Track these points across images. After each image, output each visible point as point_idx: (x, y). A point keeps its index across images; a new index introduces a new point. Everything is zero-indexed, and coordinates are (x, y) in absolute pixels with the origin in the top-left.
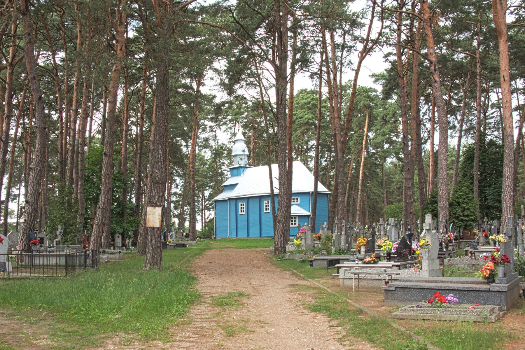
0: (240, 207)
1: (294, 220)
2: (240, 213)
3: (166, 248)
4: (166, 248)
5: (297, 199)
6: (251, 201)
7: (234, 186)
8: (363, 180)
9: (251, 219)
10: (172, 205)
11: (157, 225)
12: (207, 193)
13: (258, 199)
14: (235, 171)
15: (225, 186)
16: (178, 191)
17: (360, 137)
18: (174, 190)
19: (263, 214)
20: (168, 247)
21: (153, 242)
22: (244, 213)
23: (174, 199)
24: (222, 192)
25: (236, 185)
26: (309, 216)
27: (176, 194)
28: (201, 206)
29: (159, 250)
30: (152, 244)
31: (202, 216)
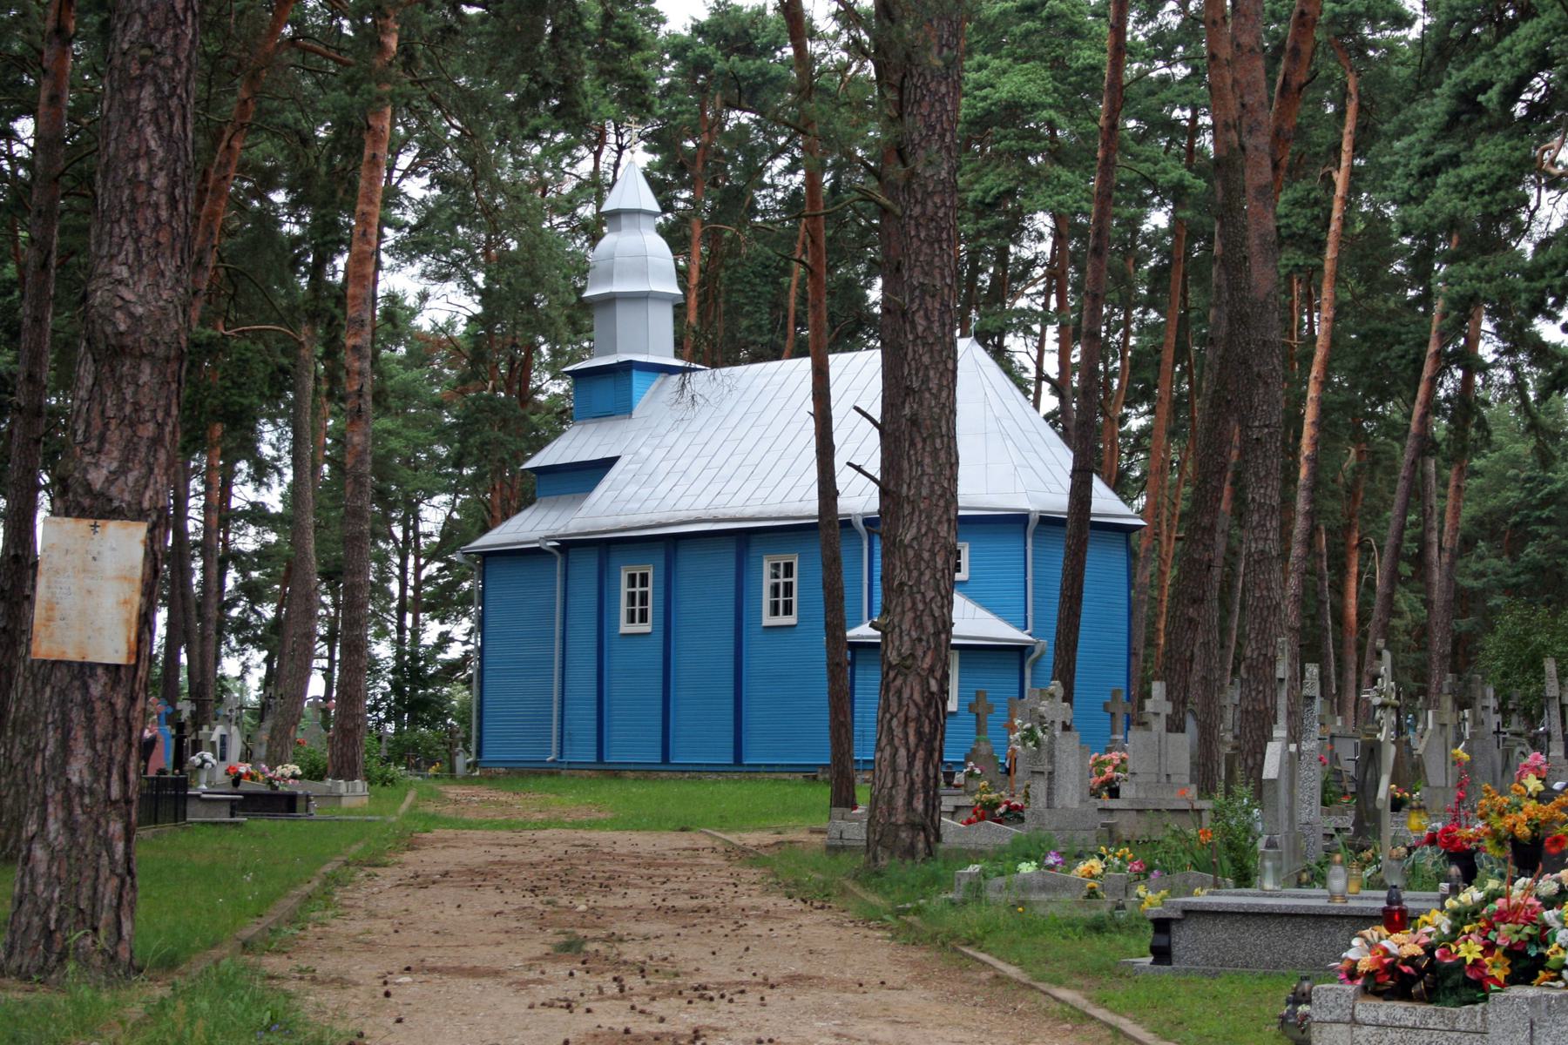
0: (624, 590)
2: (625, 628)
3: (179, 815)
4: (179, 815)
6: (689, 564)
7: (597, 469)
8: (1314, 460)
9: (681, 660)
10: (232, 578)
11: (113, 648)
12: (434, 515)
13: (725, 563)
14: (603, 391)
15: (540, 471)
16: (273, 499)
18: (243, 495)
20: (195, 813)
21: (78, 771)
22: (646, 628)
23: (247, 540)
24: (526, 501)
25: (609, 463)
26: (1019, 652)
27: (257, 514)
28: (394, 587)
29: (116, 827)
30: (66, 787)
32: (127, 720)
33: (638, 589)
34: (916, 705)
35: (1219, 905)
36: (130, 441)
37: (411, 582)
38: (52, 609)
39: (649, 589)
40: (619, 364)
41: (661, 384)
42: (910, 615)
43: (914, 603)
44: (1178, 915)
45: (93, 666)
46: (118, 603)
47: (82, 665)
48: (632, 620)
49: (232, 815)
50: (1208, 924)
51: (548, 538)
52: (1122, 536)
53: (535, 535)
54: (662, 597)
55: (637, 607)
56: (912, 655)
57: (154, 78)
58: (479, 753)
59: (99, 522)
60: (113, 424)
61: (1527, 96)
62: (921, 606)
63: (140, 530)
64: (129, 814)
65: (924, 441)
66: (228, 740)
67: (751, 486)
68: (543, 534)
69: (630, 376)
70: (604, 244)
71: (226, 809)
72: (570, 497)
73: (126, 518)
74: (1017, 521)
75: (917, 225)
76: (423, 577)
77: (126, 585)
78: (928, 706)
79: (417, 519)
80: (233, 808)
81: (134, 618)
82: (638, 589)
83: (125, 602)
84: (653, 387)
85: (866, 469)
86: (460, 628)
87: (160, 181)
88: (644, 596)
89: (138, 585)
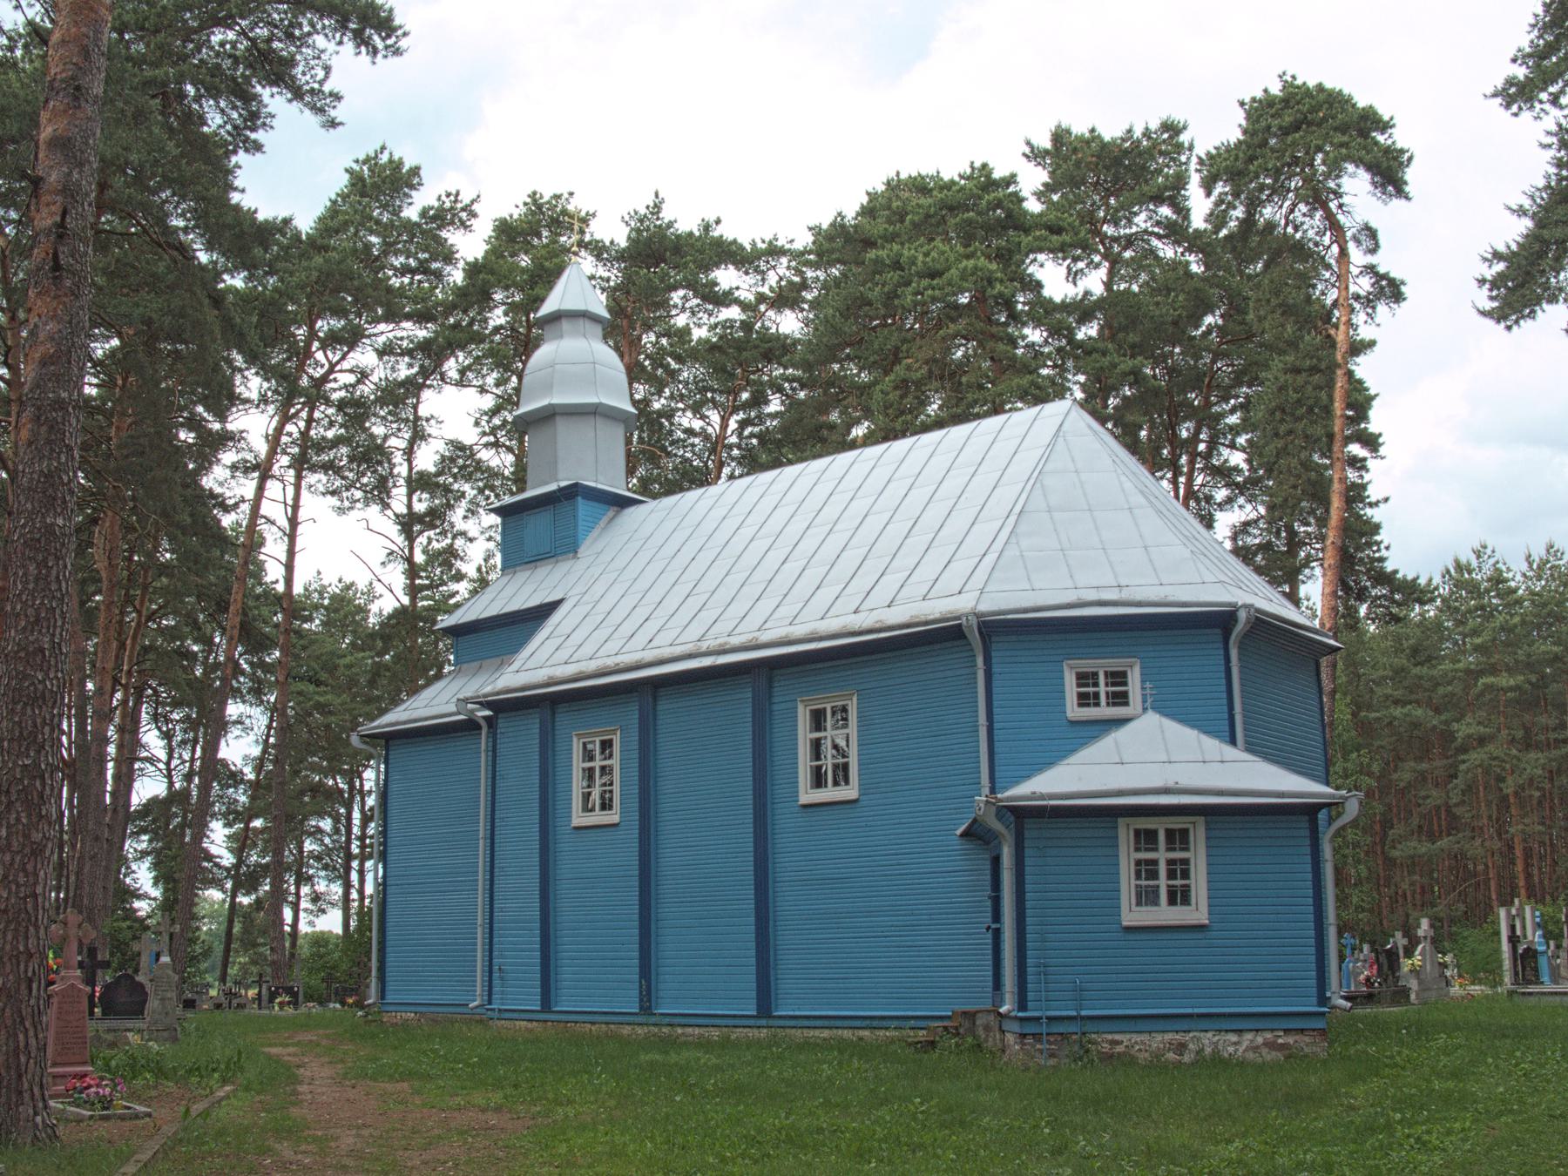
0: (578, 764)
1: (1162, 855)
5: (1118, 678)
9: (671, 858)
14: (538, 524)
17: (1314, 370)
19: (784, 823)
22: (613, 817)
25: (544, 611)
31: (347, 886)
39: (615, 762)
40: (561, 490)
41: (612, 519)
61: (353, 911)
67: (766, 606)
72: (498, 661)
84: (605, 519)
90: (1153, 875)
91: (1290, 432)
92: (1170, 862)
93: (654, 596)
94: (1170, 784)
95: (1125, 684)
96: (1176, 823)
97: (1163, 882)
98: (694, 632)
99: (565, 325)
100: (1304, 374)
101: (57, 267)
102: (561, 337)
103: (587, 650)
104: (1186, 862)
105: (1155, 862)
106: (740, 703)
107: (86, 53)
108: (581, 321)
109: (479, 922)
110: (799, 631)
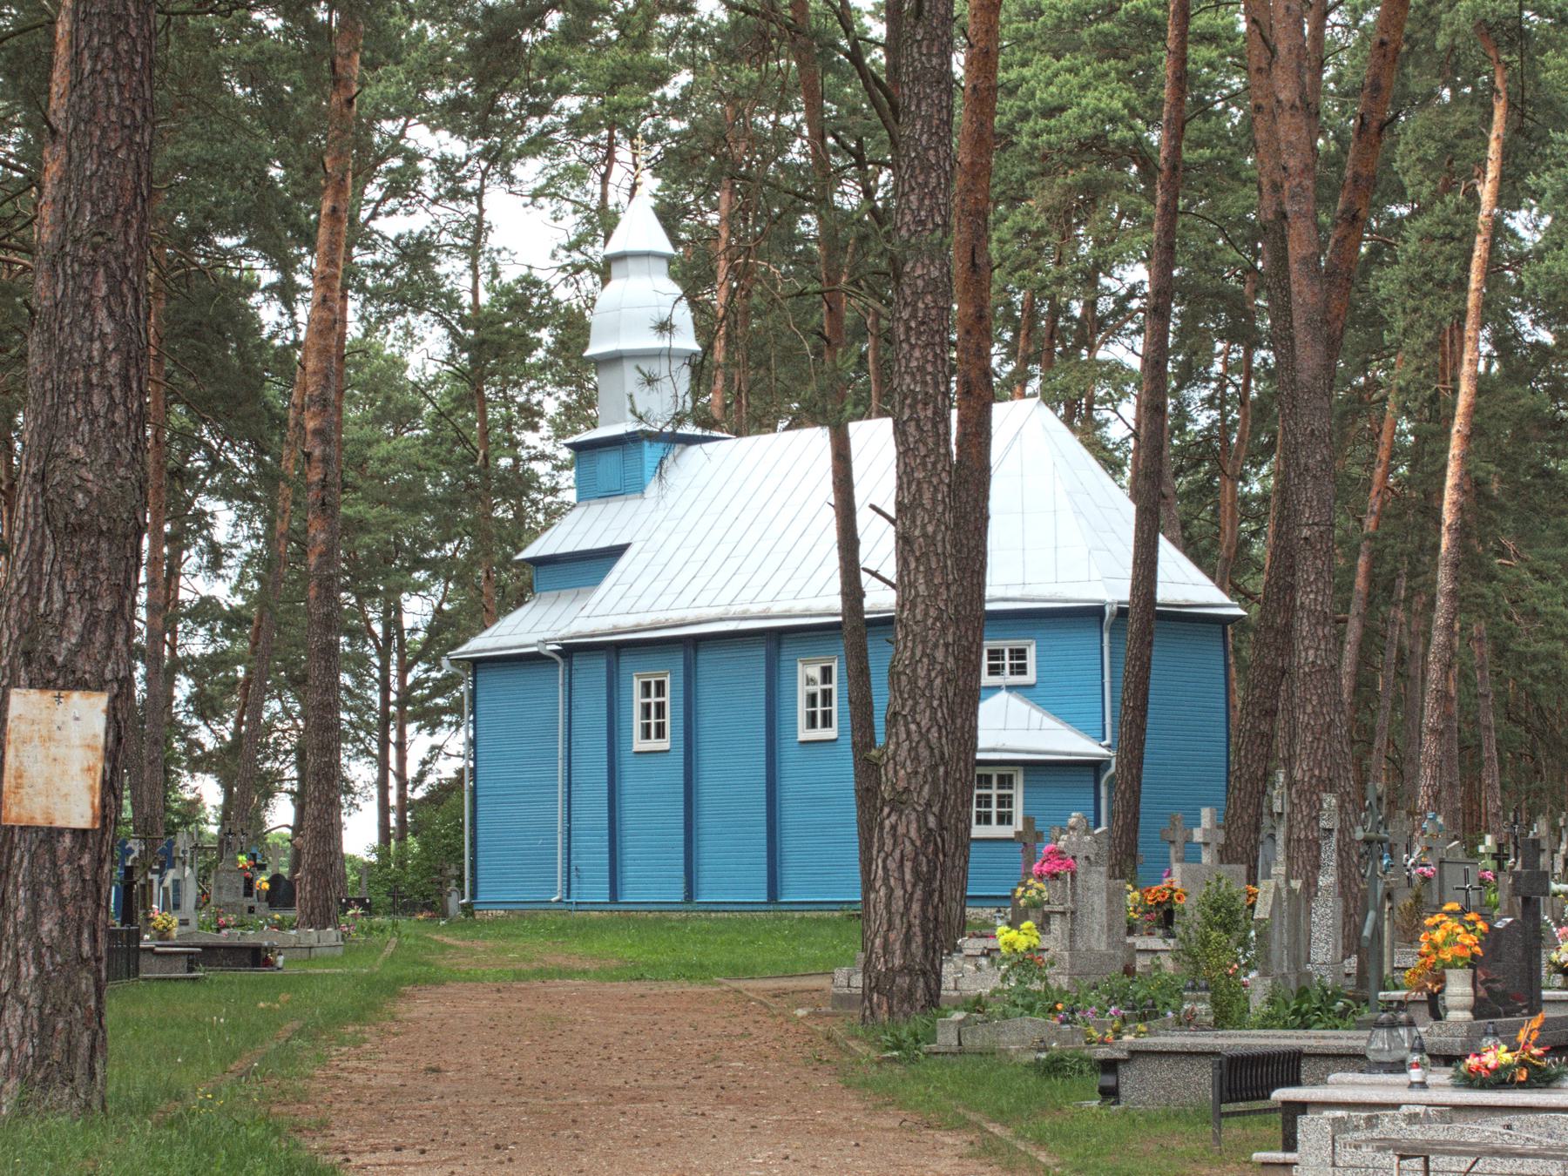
0: (638, 700)
1: (994, 792)
3: (133, 971)
4: (133, 971)
5: (1019, 654)
8: (1462, 532)
11: (78, 811)
12: (417, 611)
13: (756, 659)
14: (608, 463)
16: (221, 591)
17: (1449, 238)
18: (194, 585)
20: (150, 968)
22: (664, 744)
23: (196, 644)
25: (616, 552)
27: (206, 610)
32: (96, 882)
33: (653, 700)
34: (913, 842)
35: (1164, 1045)
36: (90, 614)
37: (395, 687)
38: (20, 777)
39: (667, 699)
42: (906, 745)
43: (908, 733)
44: (1124, 1055)
45: (61, 832)
46: (82, 770)
47: (50, 829)
48: (647, 735)
49: (190, 970)
50: (1154, 1064)
51: (545, 642)
52: (1218, 629)
53: (533, 639)
54: (681, 709)
55: (653, 721)
56: (907, 790)
57: (106, 264)
58: (474, 894)
59: (63, 693)
60: (74, 598)
62: (916, 737)
63: (101, 701)
64: (99, 971)
65: (917, 560)
66: (182, 885)
68: (541, 637)
69: (641, 447)
70: (614, 285)
71: (183, 962)
73: (89, 688)
74: (1090, 615)
75: (908, 329)
76: (410, 680)
77: (89, 754)
78: (925, 843)
79: (399, 611)
80: (190, 962)
81: (98, 785)
82: (653, 700)
83: (89, 769)
85: (881, 573)
86: (454, 740)
87: (113, 364)
88: (660, 707)
89: (100, 752)
90: (988, 804)
91: (1415, 310)
92: (999, 796)
93: (701, 554)
94: (999, 746)
95: (1024, 658)
96: (1004, 771)
97: (994, 810)
98: (725, 597)
99: (631, 263)
100: (1436, 243)
101: (324, 504)
102: (627, 276)
103: (645, 603)
104: (1010, 796)
105: (989, 796)
106: (756, 659)
107: (327, 377)
108: (645, 261)
109: (559, 829)
110: (798, 606)
